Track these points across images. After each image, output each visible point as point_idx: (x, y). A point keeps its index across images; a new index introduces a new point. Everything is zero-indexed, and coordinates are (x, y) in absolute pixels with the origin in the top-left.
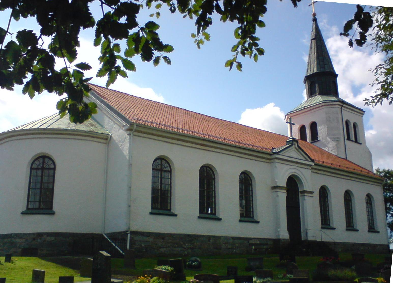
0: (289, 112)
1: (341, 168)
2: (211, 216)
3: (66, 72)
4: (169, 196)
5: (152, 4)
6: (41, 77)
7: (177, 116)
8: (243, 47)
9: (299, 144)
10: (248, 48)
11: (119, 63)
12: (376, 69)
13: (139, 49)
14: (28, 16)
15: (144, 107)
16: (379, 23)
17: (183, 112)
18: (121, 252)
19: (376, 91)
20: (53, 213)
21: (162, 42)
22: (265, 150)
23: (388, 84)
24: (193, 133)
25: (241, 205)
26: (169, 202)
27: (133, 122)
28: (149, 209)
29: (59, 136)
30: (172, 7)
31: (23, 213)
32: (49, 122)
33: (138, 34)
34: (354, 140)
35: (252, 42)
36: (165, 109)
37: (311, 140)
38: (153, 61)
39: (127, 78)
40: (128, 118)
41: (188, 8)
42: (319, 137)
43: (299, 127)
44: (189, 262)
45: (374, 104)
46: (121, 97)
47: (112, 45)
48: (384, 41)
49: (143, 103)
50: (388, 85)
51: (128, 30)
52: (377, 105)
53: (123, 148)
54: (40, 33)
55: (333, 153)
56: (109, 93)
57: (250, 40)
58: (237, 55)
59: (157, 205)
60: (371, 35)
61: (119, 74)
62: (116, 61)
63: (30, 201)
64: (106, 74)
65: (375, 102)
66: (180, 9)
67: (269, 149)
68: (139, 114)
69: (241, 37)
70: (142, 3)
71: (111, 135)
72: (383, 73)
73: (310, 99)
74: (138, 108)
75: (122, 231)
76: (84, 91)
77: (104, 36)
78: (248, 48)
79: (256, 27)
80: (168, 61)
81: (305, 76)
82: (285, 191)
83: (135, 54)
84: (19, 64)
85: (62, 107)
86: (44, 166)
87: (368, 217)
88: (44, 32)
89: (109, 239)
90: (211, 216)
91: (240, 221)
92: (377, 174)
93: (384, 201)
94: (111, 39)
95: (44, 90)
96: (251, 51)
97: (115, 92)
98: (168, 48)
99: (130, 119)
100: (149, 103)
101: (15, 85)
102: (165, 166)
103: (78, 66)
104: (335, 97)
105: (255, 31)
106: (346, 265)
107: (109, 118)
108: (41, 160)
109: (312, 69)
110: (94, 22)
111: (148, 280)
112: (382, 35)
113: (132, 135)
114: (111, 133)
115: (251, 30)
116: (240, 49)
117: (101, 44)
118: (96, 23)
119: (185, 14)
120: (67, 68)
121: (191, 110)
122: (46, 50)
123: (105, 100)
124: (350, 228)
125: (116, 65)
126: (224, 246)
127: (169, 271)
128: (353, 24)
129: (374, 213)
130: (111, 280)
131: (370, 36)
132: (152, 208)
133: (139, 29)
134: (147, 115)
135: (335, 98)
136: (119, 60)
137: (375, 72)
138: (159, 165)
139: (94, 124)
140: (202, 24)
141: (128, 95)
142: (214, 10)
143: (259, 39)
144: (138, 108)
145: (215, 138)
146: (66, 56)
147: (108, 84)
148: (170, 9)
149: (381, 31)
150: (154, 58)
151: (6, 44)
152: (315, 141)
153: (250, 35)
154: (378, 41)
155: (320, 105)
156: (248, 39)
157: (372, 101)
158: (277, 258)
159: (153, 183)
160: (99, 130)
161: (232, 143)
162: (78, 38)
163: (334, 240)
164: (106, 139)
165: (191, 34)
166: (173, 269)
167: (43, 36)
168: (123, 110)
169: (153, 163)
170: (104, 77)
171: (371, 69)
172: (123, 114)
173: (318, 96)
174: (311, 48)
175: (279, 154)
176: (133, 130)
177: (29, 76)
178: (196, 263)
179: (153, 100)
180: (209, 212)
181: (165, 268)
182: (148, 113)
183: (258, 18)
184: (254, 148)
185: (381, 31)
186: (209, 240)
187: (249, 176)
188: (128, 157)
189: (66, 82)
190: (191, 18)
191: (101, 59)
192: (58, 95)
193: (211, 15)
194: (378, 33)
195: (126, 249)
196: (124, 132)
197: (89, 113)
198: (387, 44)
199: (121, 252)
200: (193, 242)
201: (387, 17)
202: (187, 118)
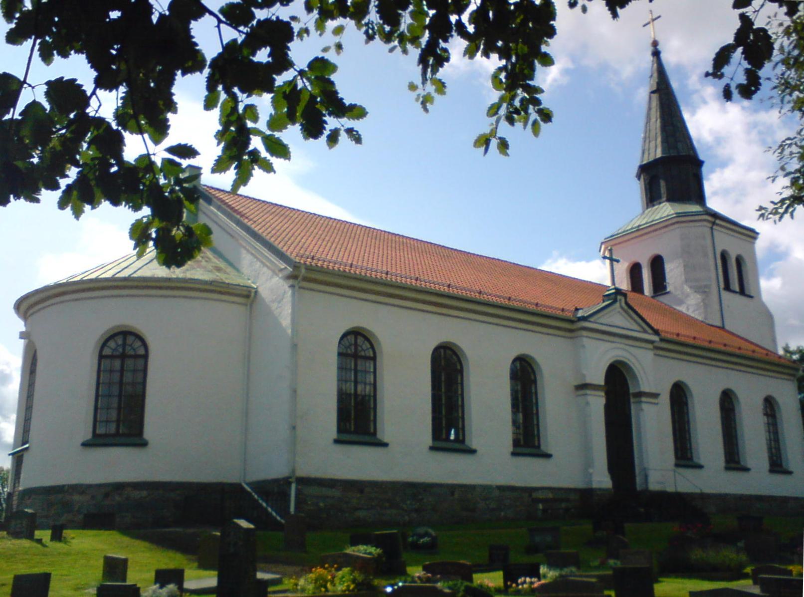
0: (608, 238)
1: (712, 346)
2: (457, 446)
3: (148, 162)
4: (372, 406)
5: (327, 27)
6: (97, 174)
7: (385, 249)
8: (509, 106)
9: (628, 299)
10: (520, 109)
11: (256, 143)
12: (781, 148)
14: (70, 54)
16: (786, 54)
17: (397, 239)
18: (278, 518)
19: (782, 192)
20: (144, 444)
21: (342, 99)
22: (561, 313)
24: (418, 282)
25: (514, 422)
27: (300, 263)
28: (333, 432)
29: (154, 292)
30: (369, 28)
31: (85, 444)
33: (292, 83)
34: (737, 289)
35: (528, 97)
36: (362, 234)
38: (326, 139)
40: (288, 254)
41: (399, 32)
42: (667, 285)
43: (628, 267)
45: (777, 217)
46: (276, 213)
47: (241, 107)
48: (796, 90)
49: (319, 225)
53: (281, 313)
54: (93, 86)
55: (696, 317)
57: (523, 93)
59: (348, 424)
62: (250, 139)
63: (98, 419)
64: (231, 166)
65: (780, 213)
67: (568, 310)
68: (311, 247)
69: (504, 86)
70: (307, 25)
71: (257, 288)
72: (796, 153)
73: (649, 210)
75: (281, 476)
77: (224, 89)
82: (603, 394)
83: (289, 124)
84: (52, 148)
85: (139, 234)
86: (127, 351)
87: (769, 443)
88: (104, 82)
90: (457, 446)
91: (514, 454)
93: (800, 412)
95: (103, 200)
96: (525, 115)
98: (356, 111)
99: (293, 257)
100: (330, 223)
101: (43, 191)
102: (364, 347)
103: (171, 150)
106: (725, 538)
107: (252, 254)
109: (652, 150)
110: (204, 60)
111: (332, 575)
112: (791, 78)
113: (297, 287)
114: (257, 284)
115: (526, 72)
116: (503, 111)
117: (219, 105)
118: (208, 63)
119: (392, 44)
120: (148, 155)
122: (107, 120)
123: (244, 220)
124: (733, 465)
125: (251, 148)
127: (373, 555)
128: (732, 54)
130: (255, 575)
131: (767, 81)
132: (340, 431)
133: (296, 73)
134: (327, 248)
135: (698, 206)
136: (257, 137)
137: (779, 153)
138: (351, 345)
139: (222, 266)
140: (431, 62)
141: (290, 208)
142: (454, 33)
144: (308, 234)
145: (462, 290)
146: (146, 132)
147: (237, 184)
150: (327, 133)
151: (23, 108)
152: (660, 293)
154: (783, 91)
155: (670, 222)
156: (519, 91)
157: (774, 211)
158: (587, 527)
159: (341, 380)
160: (231, 278)
162: (172, 94)
163: (701, 490)
165: (408, 84)
167: (99, 92)
168: (279, 239)
169: (340, 343)
170: (228, 172)
171: (770, 148)
172: (280, 247)
173: (665, 205)
174: (650, 109)
175: (589, 319)
177: (73, 173)
180: (452, 437)
181: (366, 550)
182: (329, 244)
183: (539, 48)
184: (539, 310)
185: (790, 70)
186: (453, 494)
187: (530, 365)
188: (289, 331)
189: (148, 183)
190: (405, 51)
191: (220, 136)
192: (132, 211)
193: (447, 44)
194: (783, 74)
195: (289, 512)
197: (195, 245)
199: (278, 518)
200: (420, 497)
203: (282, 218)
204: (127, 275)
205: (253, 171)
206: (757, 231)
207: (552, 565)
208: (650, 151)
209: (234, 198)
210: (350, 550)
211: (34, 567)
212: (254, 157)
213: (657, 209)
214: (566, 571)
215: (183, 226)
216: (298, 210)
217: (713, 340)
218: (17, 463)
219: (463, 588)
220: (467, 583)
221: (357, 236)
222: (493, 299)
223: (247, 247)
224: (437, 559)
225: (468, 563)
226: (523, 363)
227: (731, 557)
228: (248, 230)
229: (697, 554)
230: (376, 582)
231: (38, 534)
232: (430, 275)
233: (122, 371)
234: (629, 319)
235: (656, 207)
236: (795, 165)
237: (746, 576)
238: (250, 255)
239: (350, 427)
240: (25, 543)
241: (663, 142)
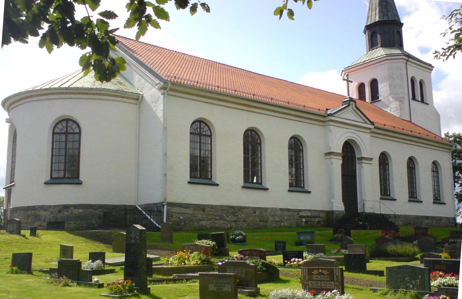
2: (257, 186)
3: (88, 21)
6: (60, 27)
9: (356, 104)
11: (149, 11)
15: (179, 62)
18: (157, 225)
19: (449, 42)
20: (80, 183)
22: (318, 111)
24: (236, 92)
34: (420, 100)
36: (203, 64)
40: (161, 75)
43: (358, 84)
49: (179, 58)
52: (448, 59)
53: (157, 109)
55: (395, 115)
64: (135, 24)
72: (459, 19)
73: (370, 52)
75: (158, 202)
81: (365, 25)
82: (341, 158)
85: (85, 63)
89: (143, 211)
90: (257, 186)
92: (446, 138)
95: (64, 43)
99: (163, 77)
102: (205, 129)
106: (408, 239)
109: (373, 17)
113: (166, 95)
120: (89, 17)
124: (437, 201)
125: (147, 13)
126: (271, 219)
130: (146, 255)
134: (183, 72)
136: (150, 7)
137: (449, 19)
139: (122, 82)
144: (172, 63)
146: (87, 3)
147: (138, 36)
150: (190, 5)
155: (383, 59)
157: (443, 54)
158: (330, 232)
160: (128, 89)
170: (133, 28)
171: (444, 16)
177: (45, 27)
180: (255, 181)
181: (207, 243)
186: (255, 213)
188: (162, 120)
189: (89, 33)
196: (157, 91)
197: (116, 69)
199: (157, 225)
200: (237, 214)
203: (157, 54)
204: (67, 86)
205: (148, 27)
206: (433, 65)
207: (310, 252)
208: (372, 17)
209: (128, 41)
210: (198, 242)
211: (22, 250)
212: (148, 19)
213: (375, 51)
214: (317, 255)
215: (109, 58)
216: (166, 49)
217: (405, 128)
218: (8, 193)
219: (260, 263)
220: (263, 261)
221: (200, 65)
222: (261, 99)
223: (137, 71)
224: (246, 248)
225: (264, 250)
226: (295, 139)
227: (409, 249)
228: (137, 60)
229: (391, 248)
230: (212, 260)
231: (23, 232)
232: (243, 88)
233: (66, 142)
234: (357, 115)
235: (374, 50)
236: (456, 27)
237: (417, 259)
238: (138, 75)
239: (197, 175)
240: (17, 237)
241: (379, 12)
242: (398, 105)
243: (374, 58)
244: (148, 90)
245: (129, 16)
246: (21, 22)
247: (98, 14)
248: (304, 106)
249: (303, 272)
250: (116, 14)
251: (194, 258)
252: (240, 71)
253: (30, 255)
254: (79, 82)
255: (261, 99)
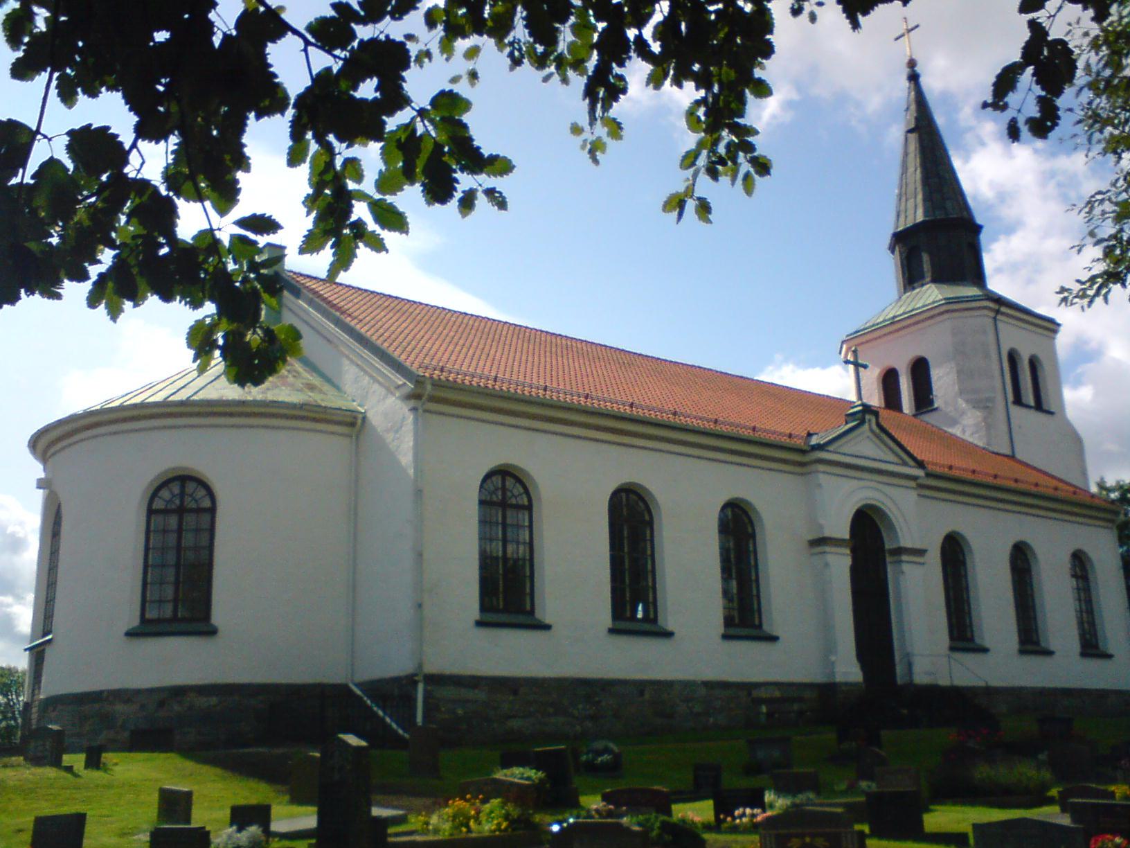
0: (851, 334)
2: (647, 627)
3: (211, 241)
4: (528, 574)
6: (141, 258)
8: (711, 154)
9: (880, 419)
10: (726, 158)
11: (360, 211)
12: (1090, 205)
13: (415, 171)
15: (452, 334)
16: (1094, 75)
17: (559, 342)
18: (400, 731)
19: (1091, 266)
20: (212, 632)
21: (479, 148)
22: (788, 441)
23: (1125, 243)
25: (726, 593)
26: (528, 590)
27: (424, 376)
28: (474, 611)
30: (514, 48)
31: (131, 634)
32: (194, 382)
33: (409, 127)
34: (1032, 403)
35: (736, 141)
37: (914, 408)
38: (457, 204)
39: (384, 252)
40: (408, 364)
41: (556, 54)
42: (934, 398)
43: (879, 374)
44: (587, 753)
45: (1086, 301)
47: (338, 162)
48: (1108, 125)
50: (1124, 248)
51: (384, 118)
52: (1094, 305)
53: (399, 447)
56: (356, 298)
57: (730, 135)
58: (696, 179)
60: (1070, 110)
61: (362, 242)
62: (352, 206)
64: (327, 243)
65: (1089, 296)
66: (532, 58)
68: (439, 354)
69: (704, 126)
71: (365, 413)
72: (1109, 213)
73: (908, 294)
74: (435, 336)
75: (402, 674)
76: (263, 294)
77: (314, 136)
78: (726, 158)
79: (746, 98)
80: (499, 201)
81: (891, 231)
82: (848, 551)
83: (405, 184)
84: (77, 223)
85: (201, 341)
86: (186, 503)
88: (146, 130)
89: (365, 698)
90: (647, 627)
91: (726, 637)
92: (1101, 494)
94: (335, 145)
95: (149, 295)
96: (733, 166)
97: (372, 296)
98: (499, 165)
99: (414, 368)
100: (465, 321)
101: (66, 283)
102: (516, 492)
103: (242, 223)
104: (978, 287)
105: (745, 109)
106: (1021, 749)
107: (358, 365)
108: (176, 489)
110: (286, 98)
111: (476, 810)
112: (1102, 108)
113: (420, 411)
114: (365, 407)
115: (733, 105)
116: (702, 161)
117: (308, 159)
118: (292, 101)
119: (547, 71)
120: (211, 230)
121: (581, 338)
122: (153, 182)
123: (346, 318)
124: (1029, 647)
125: (354, 218)
127: (533, 781)
129: (1093, 593)
130: (369, 811)
131: (1068, 113)
132: (484, 608)
134: (462, 356)
135: (975, 289)
136: (362, 203)
137: (1087, 213)
138: (497, 489)
140: (601, 94)
141: (409, 301)
142: (632, 54)
143: (755, 132)
144: (435, 336)
145: (649, 411)
146: (208, 198)
147: (335, 269)
148: (508, 56)
149: (1100, 98)
150: (458, 195)
152: (925, 410)
153: (731, 121)
154: (1091, 127)
155: (937, 311)
156: (725, 133)
157: (1081, 293)
158: (829, 736)
159: (484, 538)
160: (330, 399)
161: (695, 423)
163: (987, 683)
164: (352, 424)
165: (569, 126)
166: (543, 775)
167: (140, 143)
169: (481, 486)
171: (1075, 205)
173: (930, 287)
174: (906, 154)
175: (827, 448)
176: (424, 399)
177: (107, 257)
178: (606, 757)
179: (477, 315)
180: (640, 615)
181: (523, 774)
183: (751, 73)
184: (757, 436)
185: (1100, 98)
186: (642, 693)
188: (411, 472)
189: (211, 269)
190: (565, 80)
191: (310, 202)
193: (623, 69)
194: (1090, 103)
195: (415, 723)
196: (399, 402)
197: (278, 355)
198: (1116, 132)
199: (400, 731)
200: (597, 699)
201: (1116, 58)
202: (571, 361)
203: (398, 314)
206: (1058, 321)
207: (780, 790)
208: (908, 213)
209: (331, 288)
210: (501, 775)
211: (63, 805)
213: (918, 293)
214: (800, 798)
216: (421, 304)
219: (658, 824)
220: (665, 818)
221: (503, 338)
224: (623, 785)
225: (665, 790)
226: (736, 510)
229: (982, 772)
230: (537, 818)
231: (67, 759)
232: (605, 390)
233: (180, 530)
234: (882, 446)
235: (917, 290)
237: (1050, 801)
238: (354, 367)
239: (498, 604)
240: (50, 772)
241: (925, 200)
242: (980, 419)
243: (917, 309)
244: (379, 401)
245: (312, 225)
246: (278, 286)
247: (234, 223)
248: (716, 420)
249: (763, 838)
250: (277, 223)
251: (493, 815)
252: (599, 350)
253: (80, 819)
254: (213, 387)
255: (650, 414)
